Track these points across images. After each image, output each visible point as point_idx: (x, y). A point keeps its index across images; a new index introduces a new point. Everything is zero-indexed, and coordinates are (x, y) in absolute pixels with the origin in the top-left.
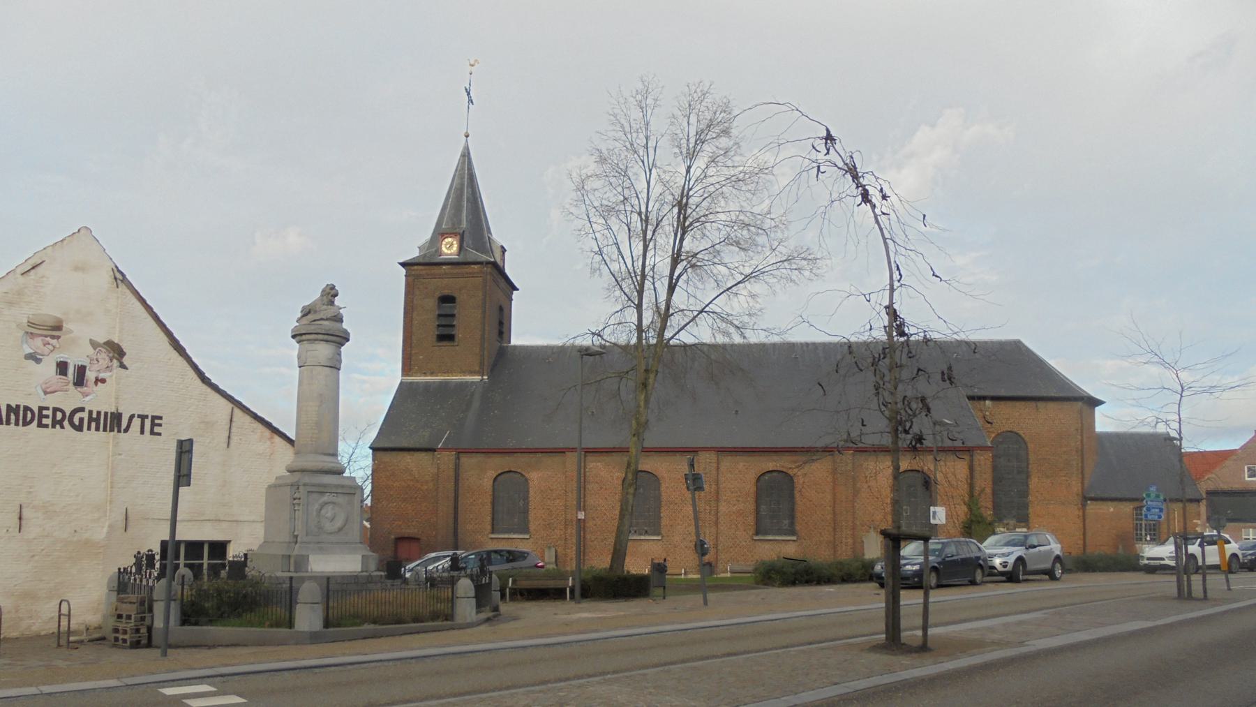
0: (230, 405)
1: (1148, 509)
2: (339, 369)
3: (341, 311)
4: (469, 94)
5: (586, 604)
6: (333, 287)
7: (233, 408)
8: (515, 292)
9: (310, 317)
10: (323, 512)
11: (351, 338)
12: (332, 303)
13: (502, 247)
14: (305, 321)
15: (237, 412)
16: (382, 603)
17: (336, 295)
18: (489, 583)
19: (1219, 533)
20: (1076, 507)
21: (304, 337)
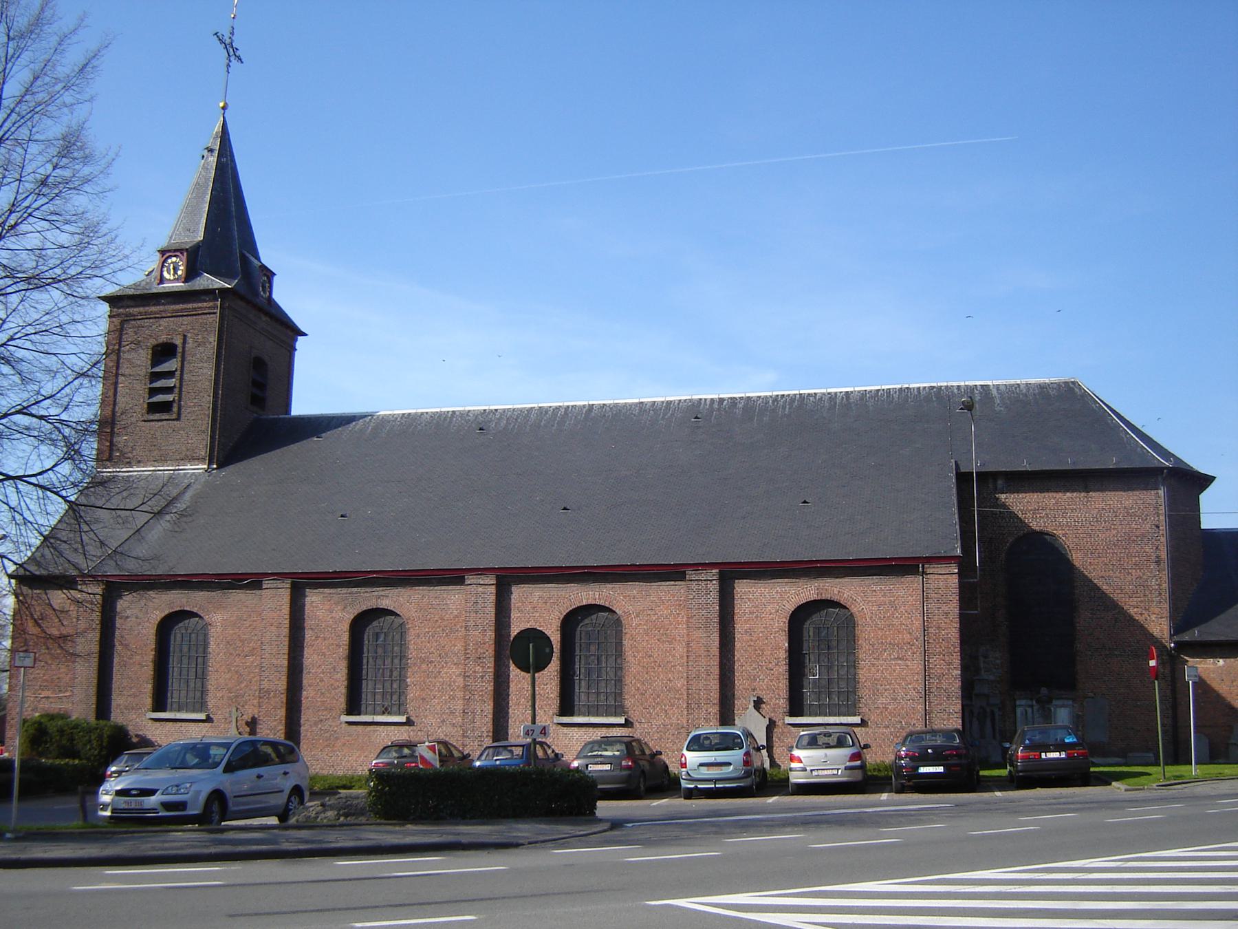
8: (299, 338)
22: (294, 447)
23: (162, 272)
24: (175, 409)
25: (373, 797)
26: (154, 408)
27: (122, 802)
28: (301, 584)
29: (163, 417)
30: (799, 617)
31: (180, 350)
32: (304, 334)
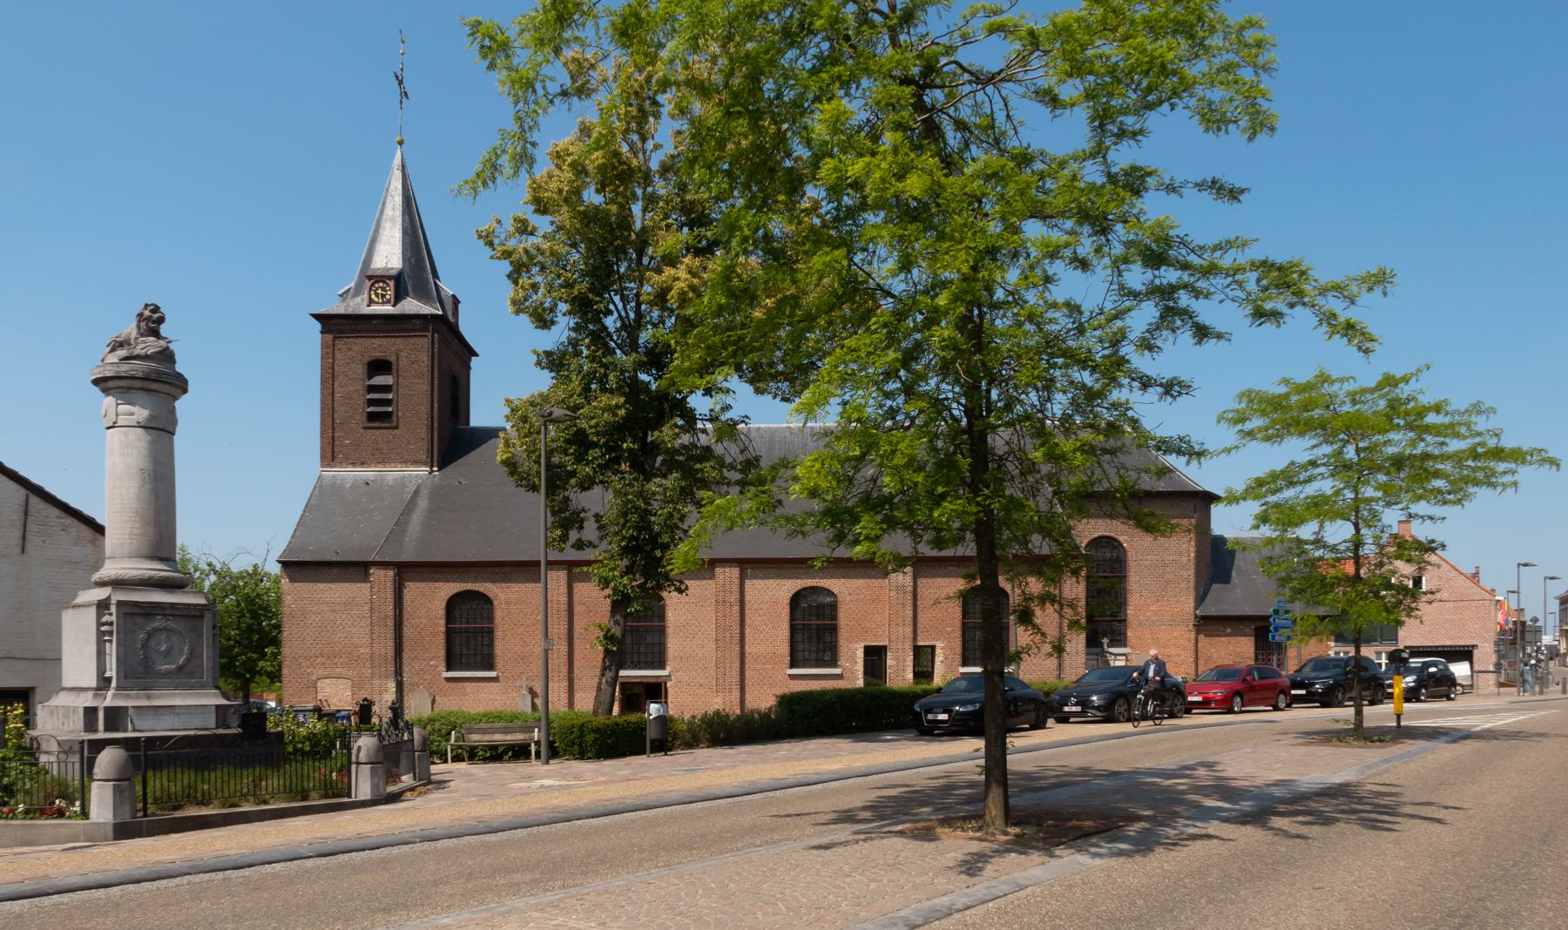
0: (22, 492)
1: (1276, 629)
2: (173, 434)
3: (171, 346)
4: (401, 83)
5: (555, 765)
6: (156, 309)
7: (27, 496)
8: (473, 358)
9: (122, 353)
10: (152, 643)
11: (190, 387)
12: (155, 333)
13: (454, 297)
14: (113, 358)
15: (35, 502)
16: (302, 775)
17: (161, 320)
18: (409, 740)
19: (1358, 650)
20: (1339, 336)
21: (111, 384)
22: (482, 447)
23: (370, 295)
24: (395, 419)
25: (1263, 519)
26: (372, 417)
27: (313, 794)
28: (405, 571)
29: (384, 425)
30: (452, 604)
31: (394, 367)
32: (477, 355)
